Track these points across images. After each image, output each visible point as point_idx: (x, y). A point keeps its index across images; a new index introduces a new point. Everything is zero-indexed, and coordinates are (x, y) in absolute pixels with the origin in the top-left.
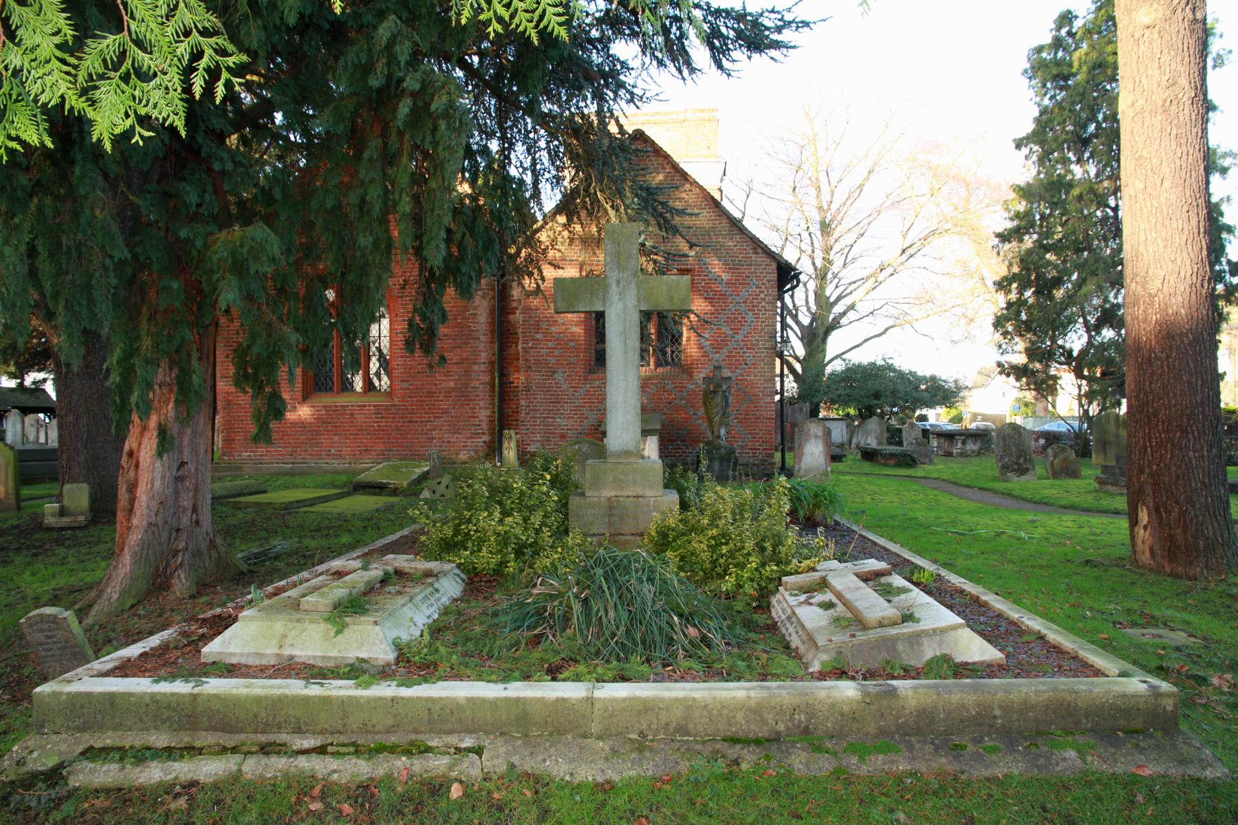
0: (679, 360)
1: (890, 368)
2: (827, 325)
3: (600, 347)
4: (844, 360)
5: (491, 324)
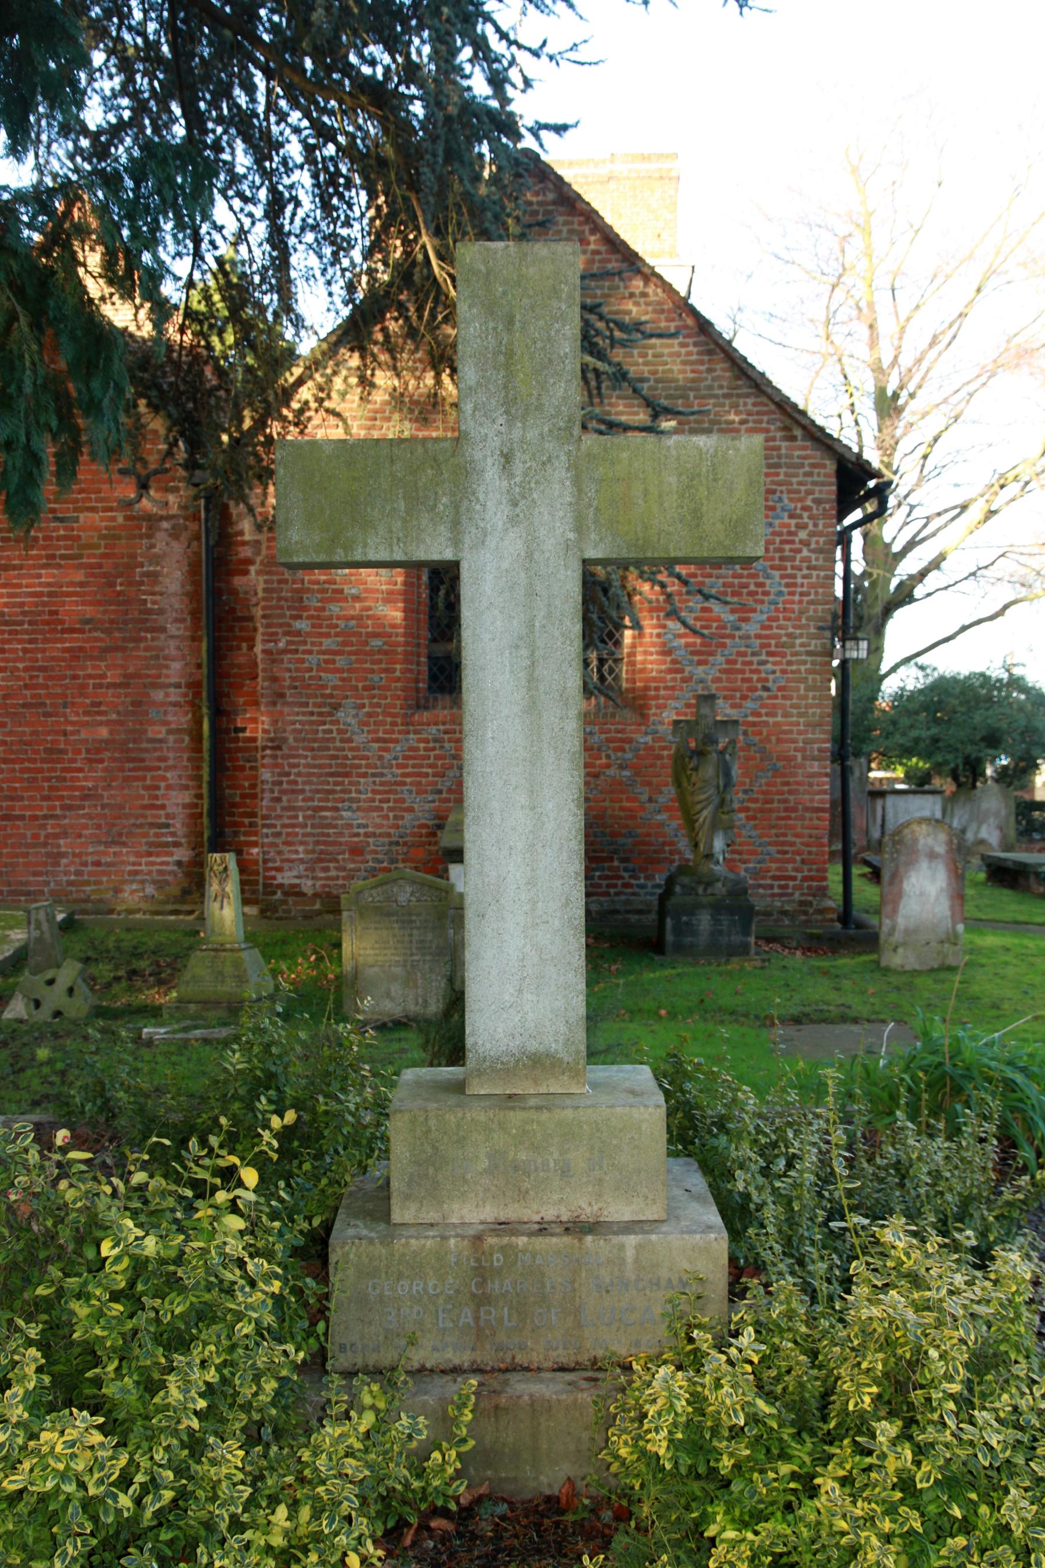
0: (617, 678)
1: (1016, 683)
2: (886, 598)
3: (440, 649)
4: (922, 668)
5: (193, 596)
